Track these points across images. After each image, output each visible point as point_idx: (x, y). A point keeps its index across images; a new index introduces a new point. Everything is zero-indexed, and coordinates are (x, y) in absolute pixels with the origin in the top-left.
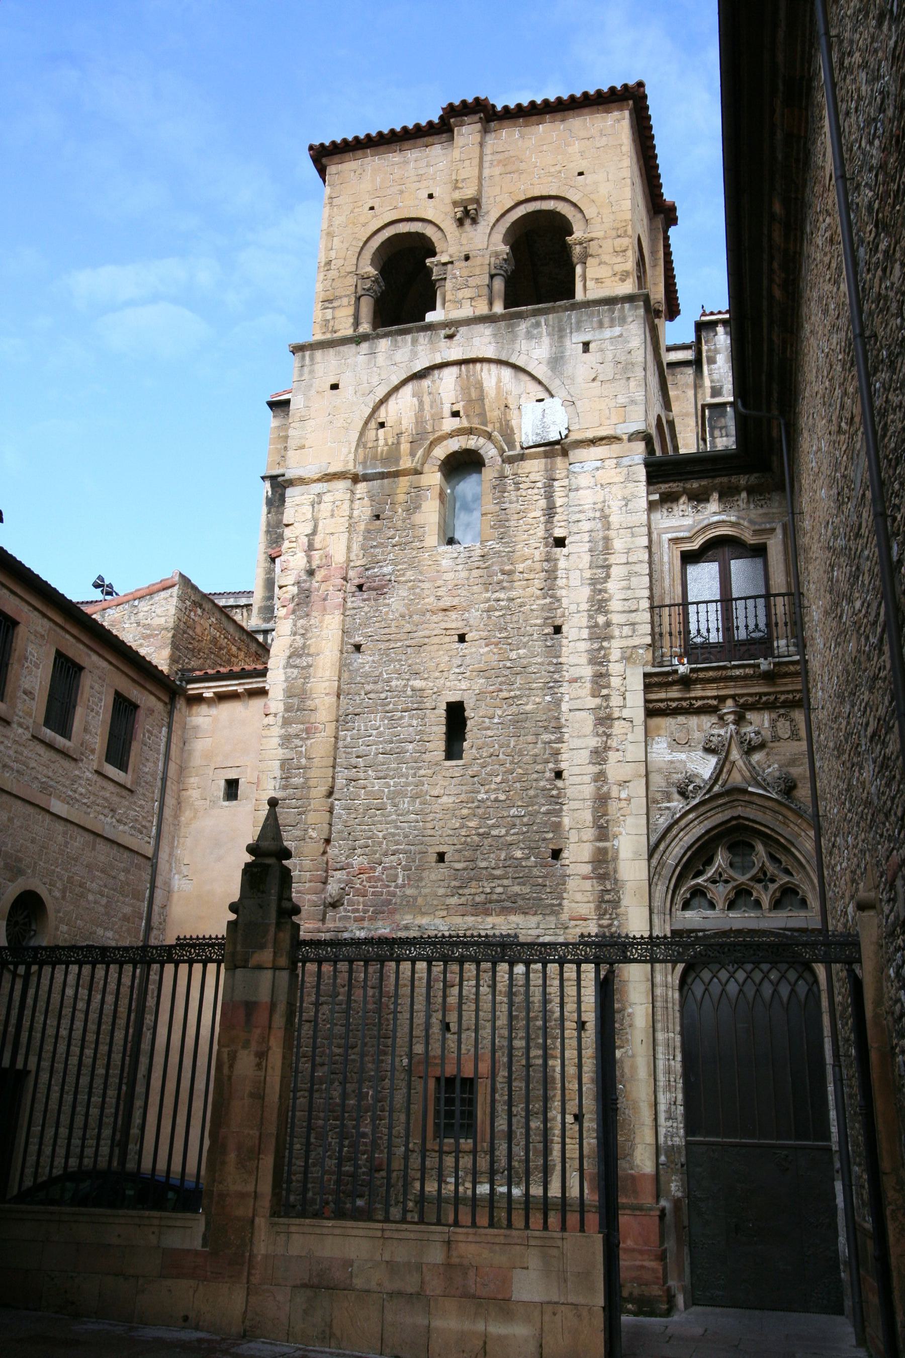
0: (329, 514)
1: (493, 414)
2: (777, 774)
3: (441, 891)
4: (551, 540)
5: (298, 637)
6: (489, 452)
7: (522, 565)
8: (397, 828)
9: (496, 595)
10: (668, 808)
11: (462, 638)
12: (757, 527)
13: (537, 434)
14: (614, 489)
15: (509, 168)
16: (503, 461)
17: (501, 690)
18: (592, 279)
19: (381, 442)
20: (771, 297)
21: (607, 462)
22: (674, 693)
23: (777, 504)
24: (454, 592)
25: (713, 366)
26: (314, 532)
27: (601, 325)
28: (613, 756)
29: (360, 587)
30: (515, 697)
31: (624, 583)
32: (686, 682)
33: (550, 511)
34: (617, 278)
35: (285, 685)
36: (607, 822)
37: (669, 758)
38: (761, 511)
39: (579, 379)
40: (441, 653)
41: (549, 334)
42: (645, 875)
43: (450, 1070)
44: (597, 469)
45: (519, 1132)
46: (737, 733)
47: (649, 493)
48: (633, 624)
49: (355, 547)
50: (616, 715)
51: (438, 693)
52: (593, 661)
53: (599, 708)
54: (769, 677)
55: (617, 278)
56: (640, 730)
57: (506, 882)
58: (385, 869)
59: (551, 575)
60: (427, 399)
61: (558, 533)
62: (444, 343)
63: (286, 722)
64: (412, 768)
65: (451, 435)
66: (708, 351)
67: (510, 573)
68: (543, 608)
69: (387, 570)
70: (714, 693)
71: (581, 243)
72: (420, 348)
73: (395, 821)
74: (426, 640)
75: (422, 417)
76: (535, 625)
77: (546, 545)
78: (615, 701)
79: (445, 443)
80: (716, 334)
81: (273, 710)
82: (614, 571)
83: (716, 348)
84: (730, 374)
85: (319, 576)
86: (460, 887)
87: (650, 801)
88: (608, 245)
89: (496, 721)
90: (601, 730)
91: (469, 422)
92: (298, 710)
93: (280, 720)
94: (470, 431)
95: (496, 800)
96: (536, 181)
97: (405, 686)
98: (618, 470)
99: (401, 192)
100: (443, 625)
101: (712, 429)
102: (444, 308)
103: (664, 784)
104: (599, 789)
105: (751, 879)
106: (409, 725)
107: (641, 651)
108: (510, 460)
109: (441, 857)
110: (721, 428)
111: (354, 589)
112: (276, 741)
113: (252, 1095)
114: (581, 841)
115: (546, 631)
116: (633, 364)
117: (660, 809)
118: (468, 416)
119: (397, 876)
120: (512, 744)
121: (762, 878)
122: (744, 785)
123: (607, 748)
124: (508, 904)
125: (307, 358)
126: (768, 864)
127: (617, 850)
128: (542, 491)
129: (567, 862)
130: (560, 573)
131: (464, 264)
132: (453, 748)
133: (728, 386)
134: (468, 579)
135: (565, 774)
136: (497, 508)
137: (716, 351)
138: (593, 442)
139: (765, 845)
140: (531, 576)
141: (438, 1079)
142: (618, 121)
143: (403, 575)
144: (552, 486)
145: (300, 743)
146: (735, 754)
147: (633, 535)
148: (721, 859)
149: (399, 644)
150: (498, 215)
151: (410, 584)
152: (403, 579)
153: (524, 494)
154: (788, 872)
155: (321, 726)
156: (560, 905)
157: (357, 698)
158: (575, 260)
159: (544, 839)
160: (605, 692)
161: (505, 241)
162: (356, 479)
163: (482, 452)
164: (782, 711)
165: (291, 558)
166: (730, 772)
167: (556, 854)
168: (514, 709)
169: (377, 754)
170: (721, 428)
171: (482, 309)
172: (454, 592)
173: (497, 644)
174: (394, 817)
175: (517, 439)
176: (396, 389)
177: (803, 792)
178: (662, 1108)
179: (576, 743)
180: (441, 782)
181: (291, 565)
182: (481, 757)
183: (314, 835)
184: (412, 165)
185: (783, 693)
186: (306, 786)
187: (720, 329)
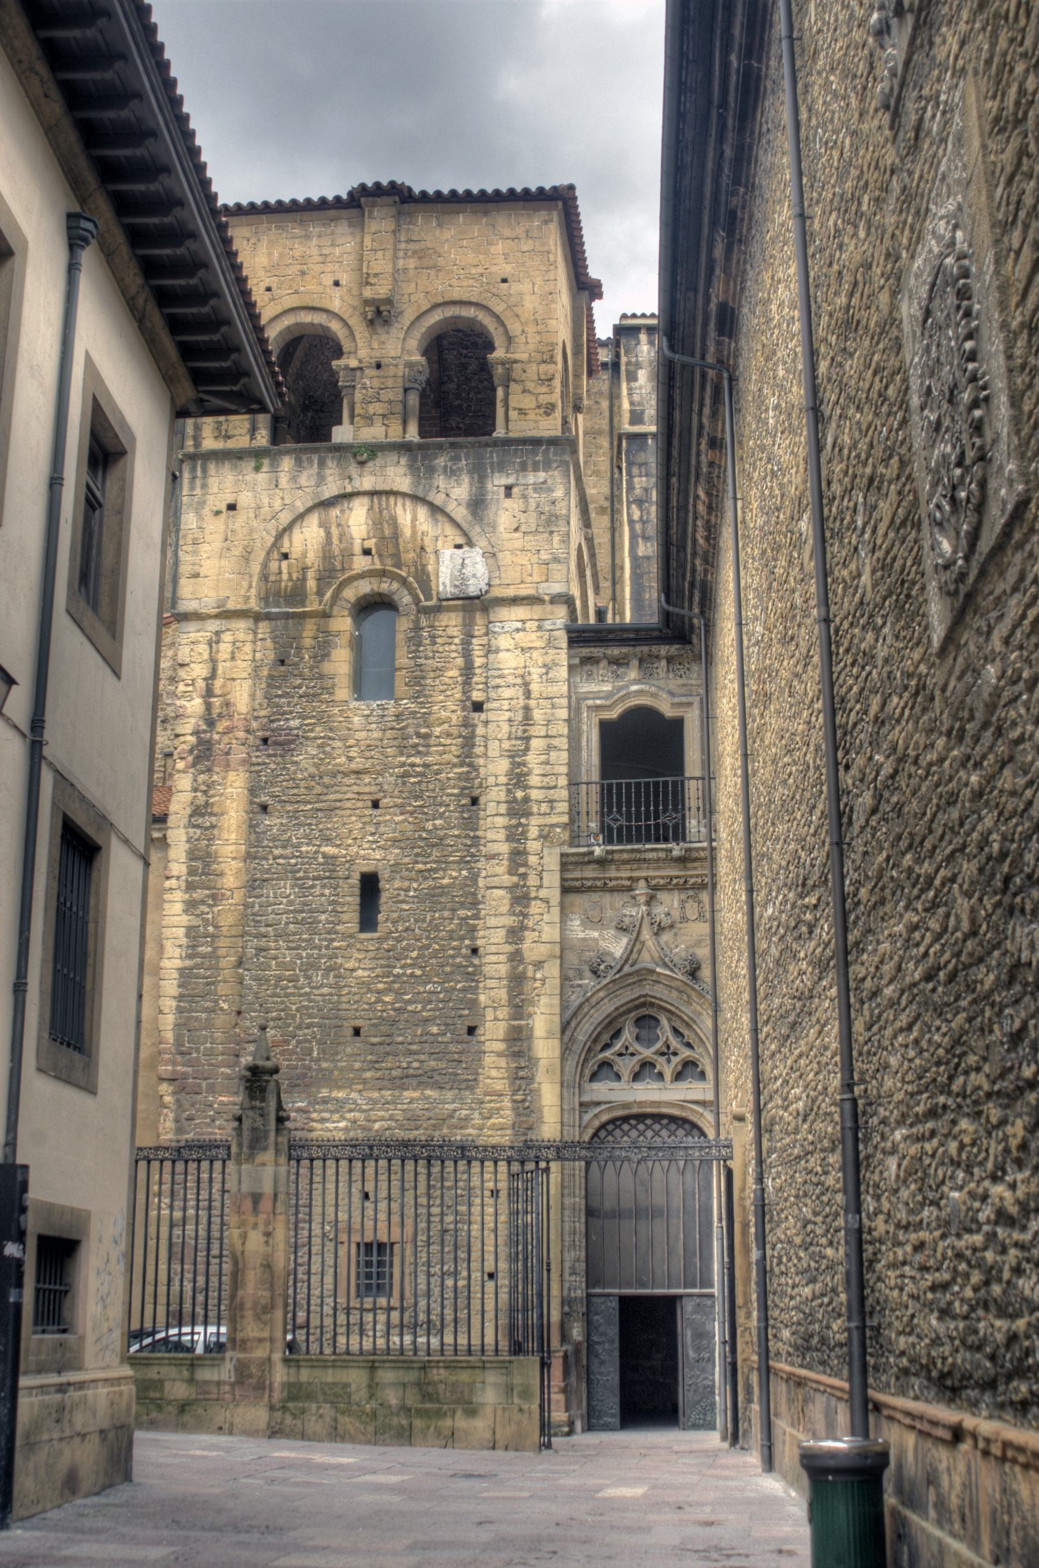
0: (228, 656)
1: (410, 556)
2: (683, 954)
3: (357, 1065)
4: (468, 704)
5: (199, 794)
6: (405, 599)
7: (439, 729)
8: (310, 1001)
9: (412, 759)
10: (580, 986)
11: (376, 805)
12: (676, 700)
13: (456, 586)
14: (535, 654)
15: (426, 262)
16: (419, 611)
17: (417, 862)
18: (515, 409)
19: (285, 576)
20: (695, 541)
21: (528, 625)
22: (590, 872)
23: (695, 675)
24: (368, 754)
25: (634, 385)
26: (213, 675)
27: (524, 468)
28: (529, 936)
29: (265, 741)
30: (431, 870)
31: (543, 758)
32: (602, 863)
33: (468, 670)
34: (542, 411)
35: (187, 846)
36: (523, 1001)
37: (581, 935)
38: (680, 681)
39: (501, 529)
40: (354, 818)
41: (469, 472)
42: (557, 1053)
43: (369, 1237)
44: (518, 630)
45: (436, 1291)
46: (648, 914)
47: (570, 657)
48: (551, 801)
49: (259, 694)
50: (533, 895)
51: (352, 862)
52: (509, 838)
53: (516, 886)
54: (683, 860)
55: (542, 411)
56: (556, 911)
57: (422, 1057)
58: (299, 1042)
59: (469, 742)
60: (335, 531)
61: (477, 696)
62: (353, 469)
63: (190, 887)
64: (325, 940)
65: (362, 576)
66: (628, 363)
67: (426, 736)
68: (460, 777)
69: (295, 723)
70: (628, 874)
71: (503, 364)
72: (328, 472)
73: (306, 994)
74: (338, 804)
75: (330, 551)
76: (452, 795)
77: (464, 709)
78: (532, 880)
79: (355, 584)
80: (638, 343)
81: (175, 873)
82: (535, 743)
83: (637, 361)
84: (654, 396)
85: (221, 727)
86: (377, 1062)
87: (564, 978)
88: (532, 369)
89: (412, 894)
90: (518, 909)
91: (382, 563)
92: (203, 874)
93: (183, 885)
94: (383, 574)
95: (412, 975)
96: (454, 282)
97: (316, 852)
98: (539, 634)
99: (303, 273)
100: (355, 788)
101: (630, 464)
102: (352, 423)
103: (576, 962)
104: (514, 968)
105: (655, 1053)
106: (321, 894)
107: (558, 830)
108: (426, 611)
109: (357, 1032)
110: (640, 465)
111: (258, 742)
112: (178, 907)
113: (262, 1265)
114: (496, 1019)
115: (463, 802)
116: (557, 516)
117: (572, 986)
118: (380, 556)
119: (311, 1050)
120: (428, 918)
121: (667, 1053)
122: (652, 966)
123: (523, 928)
124: (425, 1079)
125: (199, 469)
126: (671, 1038)
127: (532, 1030)
128: (460, 648)
129: (483, 1039)
130: (478, 740)
131: (374, 372)
132: (368, 920)
133: (651, 411)
134: (381, 740)
135: (481, 951)
136: (412, 662)
137: (638, 365)
138: (515, 601)
139: (669, 1020)
140: (449, 742)
141: (358, 1244)
142: (546, 222)
143: (312, 731)
144: (471, 643)
145: (207, 910)
146: (646, 935)
147: (553, 707)
148: (628, 1035)
149: (309, 807)
150: (412, 318)
151: (319, 741)
152: (313, 735)
153: (441, 649)
154: (689, 1045)
155: (229, 893)
156: (475, 1080)
157: (264, 862)
158: (496, 381)
159: (461, 1016)
160: (522, 870)
161: (425, 353)
162: (258, 617)
163: (396, 597)
164: (691, 893)
165: (187, 704)
166: (640, 952)
167: (471, 1030)
168: (431, 883)
169: (287, 924)
170: (640, 465)
171: (395, 433)
172: (368, 754)
173: (412, 813)
174: (307, 990)
175: (434, 587)
176: (301, 517)
177: (706, 973)
178: (567, 1265)
179: (492, 921)
180: (356, 955)
181: (189, 711)
182: (397, 931)
183: (225, 1006)
184: (315, 241)
185: (692, 876)
186: (213, 955)
187: (643, 337)
